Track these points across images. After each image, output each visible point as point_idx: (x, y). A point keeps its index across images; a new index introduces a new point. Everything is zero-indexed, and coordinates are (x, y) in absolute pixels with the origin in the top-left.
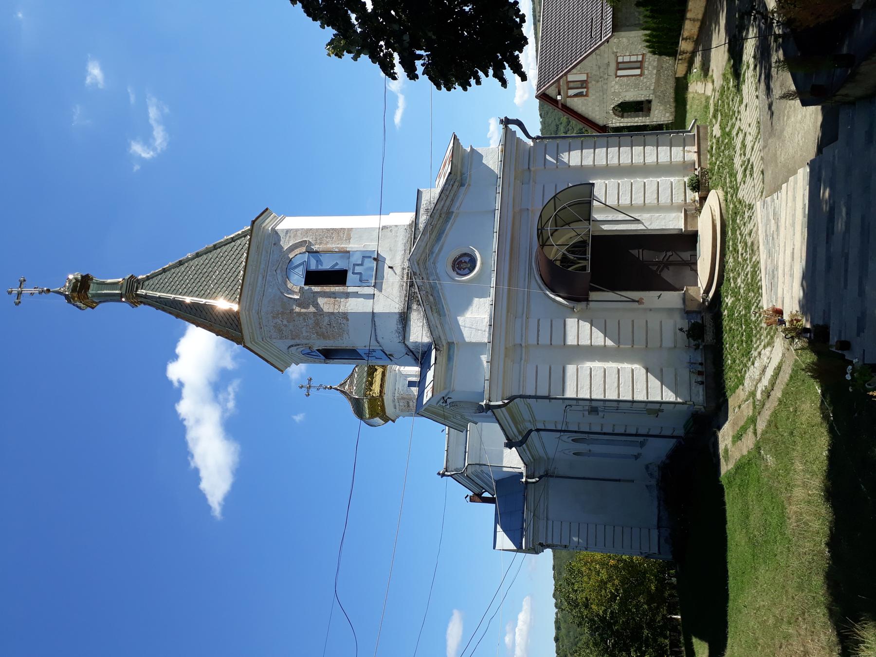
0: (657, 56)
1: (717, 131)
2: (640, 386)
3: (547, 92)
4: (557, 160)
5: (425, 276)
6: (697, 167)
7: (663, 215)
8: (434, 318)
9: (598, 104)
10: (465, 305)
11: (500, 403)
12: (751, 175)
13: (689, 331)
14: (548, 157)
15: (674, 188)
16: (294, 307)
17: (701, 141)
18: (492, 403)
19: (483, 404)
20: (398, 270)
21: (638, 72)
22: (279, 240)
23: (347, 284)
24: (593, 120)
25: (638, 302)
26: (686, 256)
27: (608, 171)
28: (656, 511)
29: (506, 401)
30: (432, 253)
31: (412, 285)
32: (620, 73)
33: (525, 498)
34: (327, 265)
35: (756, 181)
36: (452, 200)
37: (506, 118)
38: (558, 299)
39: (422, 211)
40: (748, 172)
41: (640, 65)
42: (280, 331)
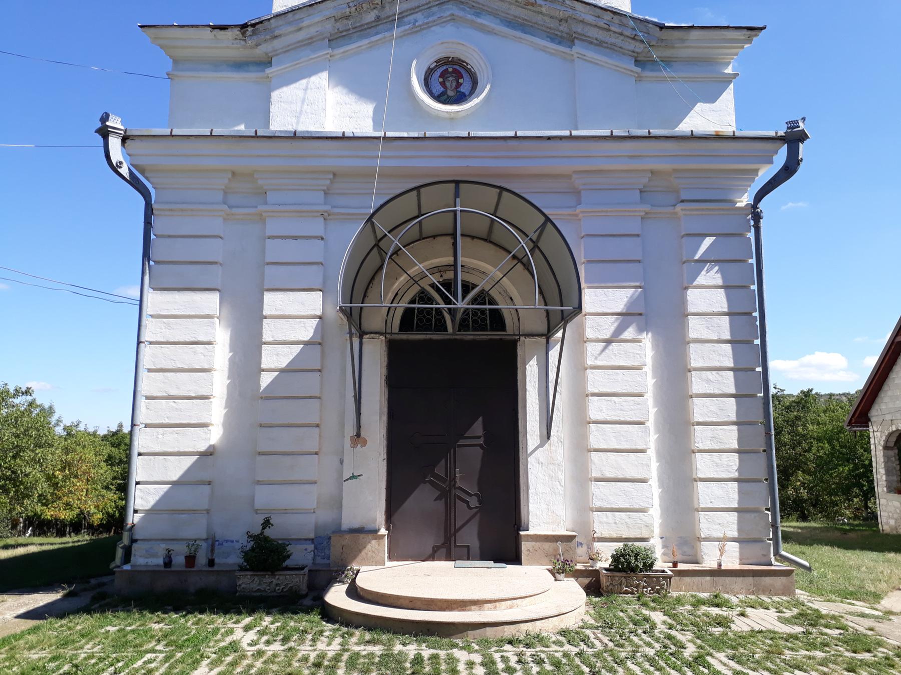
4: (703, 261)
10: (359, 87)
13: (266, 539)
14: (708, 241)
17: (750, 579)
24: (878, 400)
25: (358, 437)
26: (470, 536)
30: (478, 15)
36: (600, 44)
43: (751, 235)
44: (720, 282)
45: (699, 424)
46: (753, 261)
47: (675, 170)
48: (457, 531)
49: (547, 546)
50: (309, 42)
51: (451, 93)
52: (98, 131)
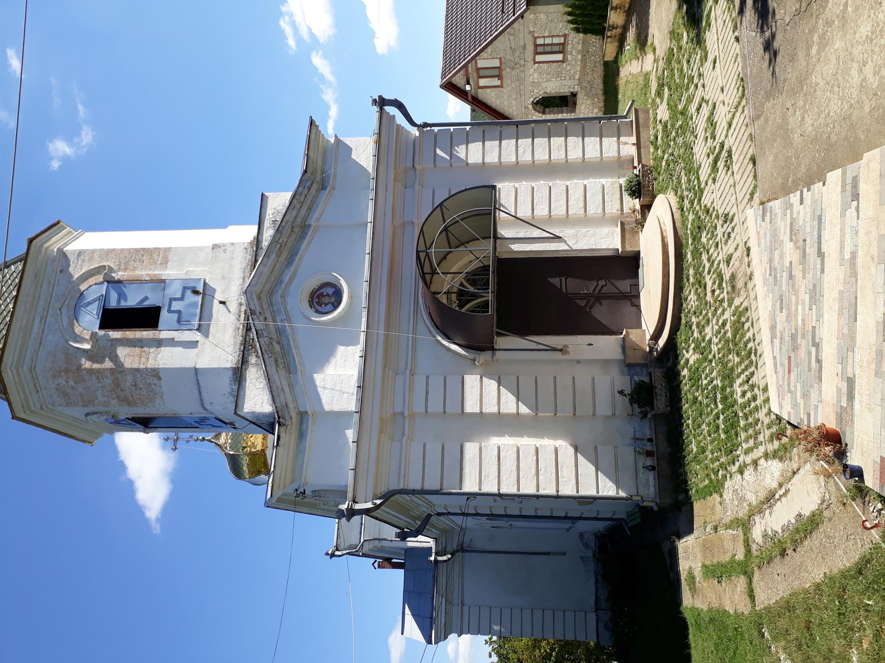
0: (581, 35)
1: (663, 113)
2: (567, 472)
3: (454, 81)
4: (451, 155)
5: (268, 315)
6: (636, 164)
7: (592, 230)
8: (281, 379)
9: (514, 97)
10: (325, 356)
11: (369, 505)
12: (728, 167)
13: (631, 395)
14: (439, 152)
15: (608, 193)
16: (83, 361)
18: (357, 507)
19: (344, 507)
20: (233, 306)
21: (559, 57)
22: (68, 266)
23: (160, 326)
26: (624, 285)
27: (518, 171)
28: (593, 589)
29: (378, 502)
30: (281, 282)
31: (248, 329)
32: (539, 58)
33: (435, 579)
34: (132, 300)
35: (737, 177)
36: (310, 209)
37: (380, 97)
38: (454, 347)
39: (267, 223)
40: (721, 164)
41: (562, 49)
42: (65, 395)
43: (436, 129)
44: (464, 146)
45: (550, 157)
46: (452, 128)
47: (395, 168)
48: (621, 292)
49: (627, 236)
50: (291, 386)
51: (333, 300)
52: (331, 558)
